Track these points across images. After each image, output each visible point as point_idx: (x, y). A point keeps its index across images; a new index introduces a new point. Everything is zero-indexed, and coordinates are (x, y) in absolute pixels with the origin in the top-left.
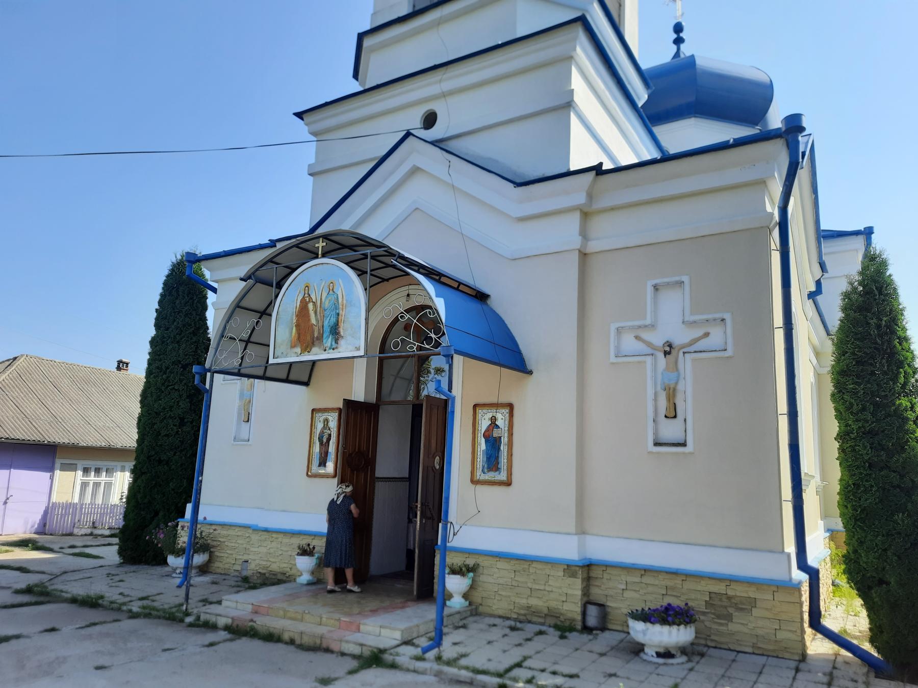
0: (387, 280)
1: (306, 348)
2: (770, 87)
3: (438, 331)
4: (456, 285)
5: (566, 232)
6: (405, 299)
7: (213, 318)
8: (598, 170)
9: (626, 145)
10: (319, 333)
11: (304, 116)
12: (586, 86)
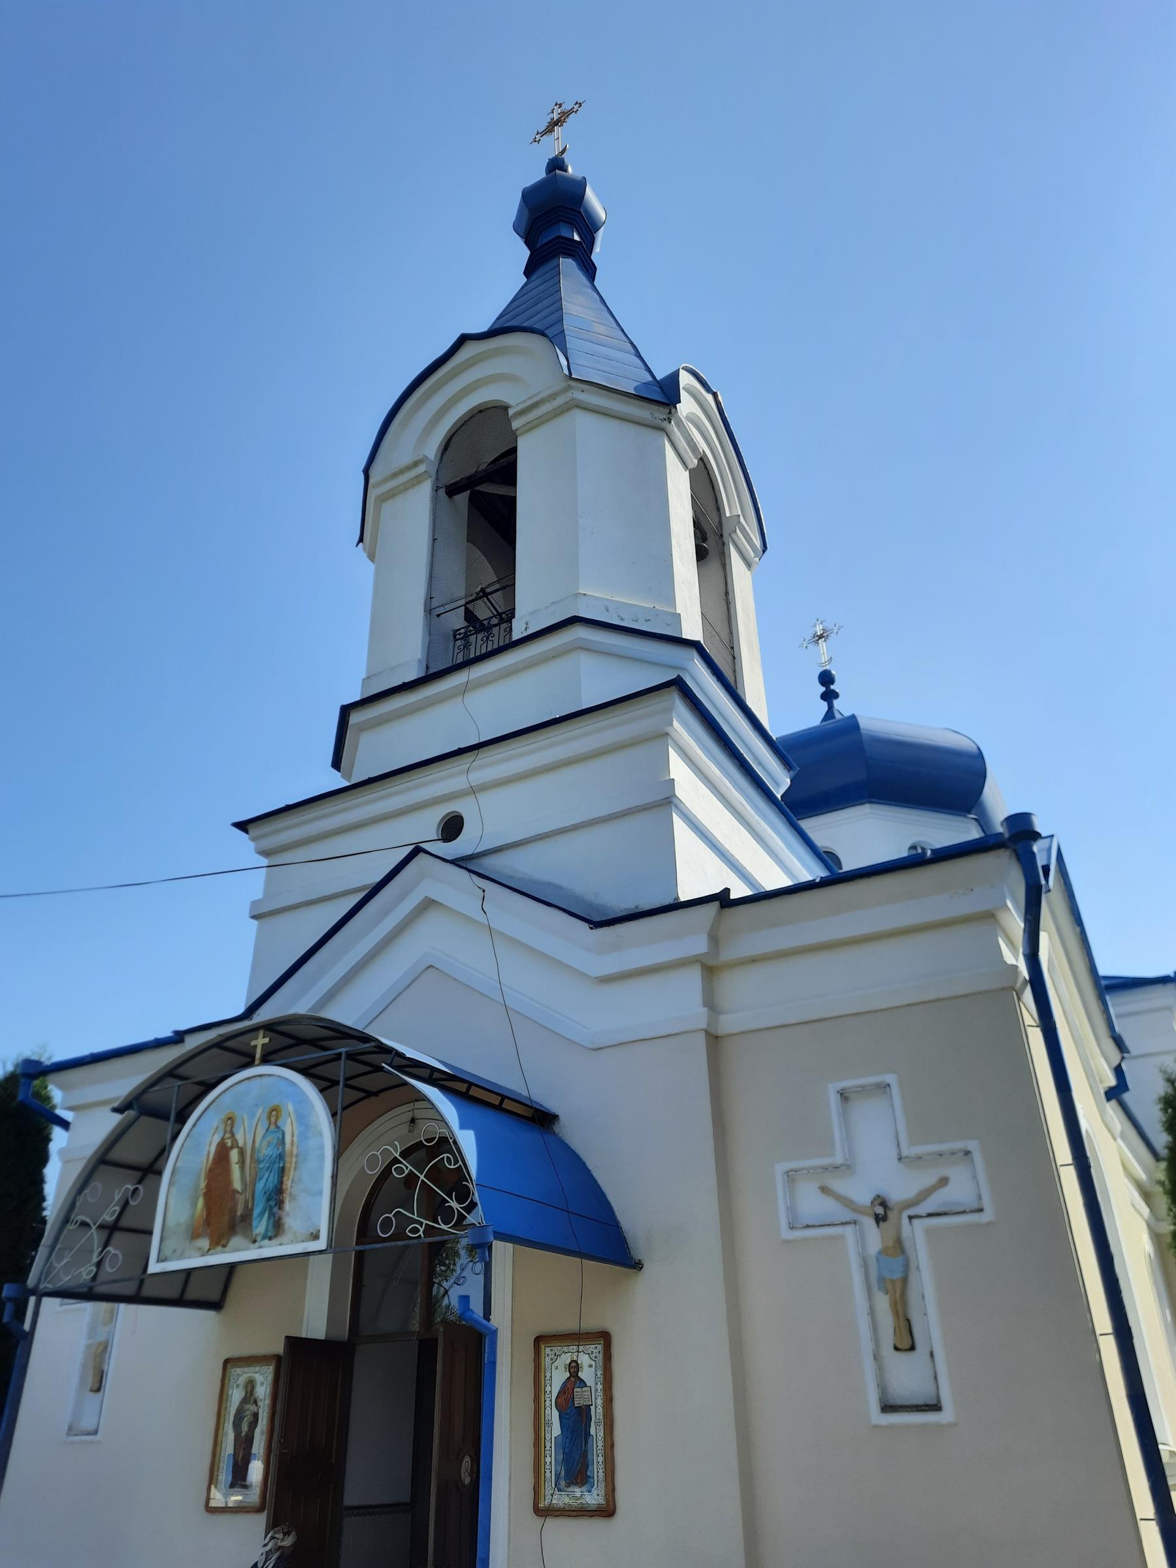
0: (376, 1094)
1: (219, 1241)
2: (980, 755)
3: (463, 1195)
4: (496, 1100)
5: (678, 1002)
6: (405, 1129)
7: (56, 1181)
8: (723, 899)
9: (767, 860)
10: (246, 1206)
11: (250, 827)
12: (692, 778)
